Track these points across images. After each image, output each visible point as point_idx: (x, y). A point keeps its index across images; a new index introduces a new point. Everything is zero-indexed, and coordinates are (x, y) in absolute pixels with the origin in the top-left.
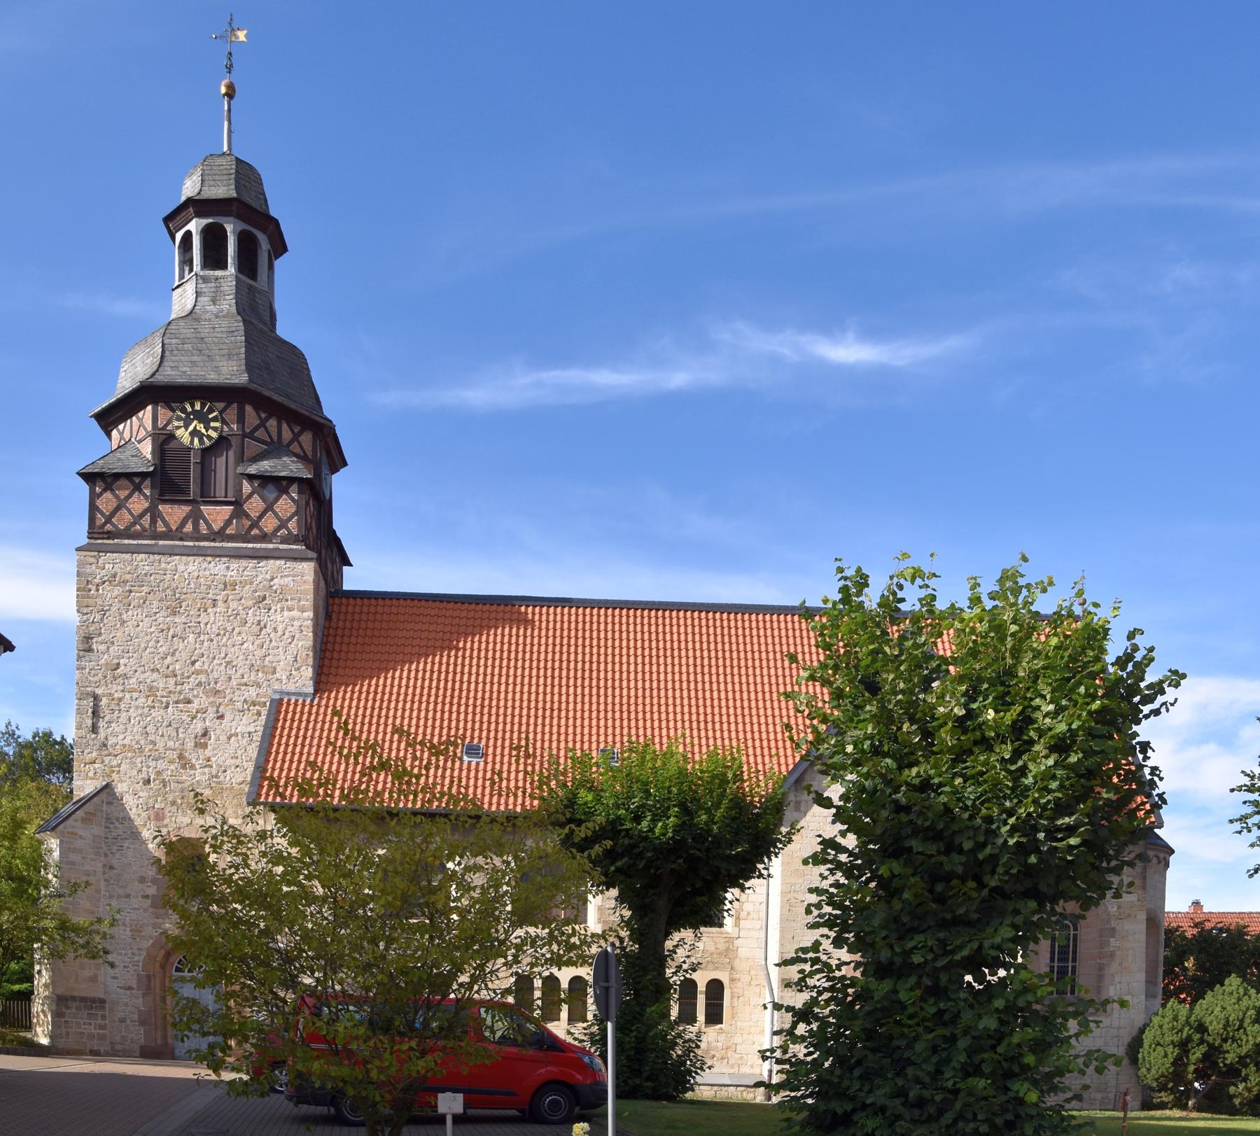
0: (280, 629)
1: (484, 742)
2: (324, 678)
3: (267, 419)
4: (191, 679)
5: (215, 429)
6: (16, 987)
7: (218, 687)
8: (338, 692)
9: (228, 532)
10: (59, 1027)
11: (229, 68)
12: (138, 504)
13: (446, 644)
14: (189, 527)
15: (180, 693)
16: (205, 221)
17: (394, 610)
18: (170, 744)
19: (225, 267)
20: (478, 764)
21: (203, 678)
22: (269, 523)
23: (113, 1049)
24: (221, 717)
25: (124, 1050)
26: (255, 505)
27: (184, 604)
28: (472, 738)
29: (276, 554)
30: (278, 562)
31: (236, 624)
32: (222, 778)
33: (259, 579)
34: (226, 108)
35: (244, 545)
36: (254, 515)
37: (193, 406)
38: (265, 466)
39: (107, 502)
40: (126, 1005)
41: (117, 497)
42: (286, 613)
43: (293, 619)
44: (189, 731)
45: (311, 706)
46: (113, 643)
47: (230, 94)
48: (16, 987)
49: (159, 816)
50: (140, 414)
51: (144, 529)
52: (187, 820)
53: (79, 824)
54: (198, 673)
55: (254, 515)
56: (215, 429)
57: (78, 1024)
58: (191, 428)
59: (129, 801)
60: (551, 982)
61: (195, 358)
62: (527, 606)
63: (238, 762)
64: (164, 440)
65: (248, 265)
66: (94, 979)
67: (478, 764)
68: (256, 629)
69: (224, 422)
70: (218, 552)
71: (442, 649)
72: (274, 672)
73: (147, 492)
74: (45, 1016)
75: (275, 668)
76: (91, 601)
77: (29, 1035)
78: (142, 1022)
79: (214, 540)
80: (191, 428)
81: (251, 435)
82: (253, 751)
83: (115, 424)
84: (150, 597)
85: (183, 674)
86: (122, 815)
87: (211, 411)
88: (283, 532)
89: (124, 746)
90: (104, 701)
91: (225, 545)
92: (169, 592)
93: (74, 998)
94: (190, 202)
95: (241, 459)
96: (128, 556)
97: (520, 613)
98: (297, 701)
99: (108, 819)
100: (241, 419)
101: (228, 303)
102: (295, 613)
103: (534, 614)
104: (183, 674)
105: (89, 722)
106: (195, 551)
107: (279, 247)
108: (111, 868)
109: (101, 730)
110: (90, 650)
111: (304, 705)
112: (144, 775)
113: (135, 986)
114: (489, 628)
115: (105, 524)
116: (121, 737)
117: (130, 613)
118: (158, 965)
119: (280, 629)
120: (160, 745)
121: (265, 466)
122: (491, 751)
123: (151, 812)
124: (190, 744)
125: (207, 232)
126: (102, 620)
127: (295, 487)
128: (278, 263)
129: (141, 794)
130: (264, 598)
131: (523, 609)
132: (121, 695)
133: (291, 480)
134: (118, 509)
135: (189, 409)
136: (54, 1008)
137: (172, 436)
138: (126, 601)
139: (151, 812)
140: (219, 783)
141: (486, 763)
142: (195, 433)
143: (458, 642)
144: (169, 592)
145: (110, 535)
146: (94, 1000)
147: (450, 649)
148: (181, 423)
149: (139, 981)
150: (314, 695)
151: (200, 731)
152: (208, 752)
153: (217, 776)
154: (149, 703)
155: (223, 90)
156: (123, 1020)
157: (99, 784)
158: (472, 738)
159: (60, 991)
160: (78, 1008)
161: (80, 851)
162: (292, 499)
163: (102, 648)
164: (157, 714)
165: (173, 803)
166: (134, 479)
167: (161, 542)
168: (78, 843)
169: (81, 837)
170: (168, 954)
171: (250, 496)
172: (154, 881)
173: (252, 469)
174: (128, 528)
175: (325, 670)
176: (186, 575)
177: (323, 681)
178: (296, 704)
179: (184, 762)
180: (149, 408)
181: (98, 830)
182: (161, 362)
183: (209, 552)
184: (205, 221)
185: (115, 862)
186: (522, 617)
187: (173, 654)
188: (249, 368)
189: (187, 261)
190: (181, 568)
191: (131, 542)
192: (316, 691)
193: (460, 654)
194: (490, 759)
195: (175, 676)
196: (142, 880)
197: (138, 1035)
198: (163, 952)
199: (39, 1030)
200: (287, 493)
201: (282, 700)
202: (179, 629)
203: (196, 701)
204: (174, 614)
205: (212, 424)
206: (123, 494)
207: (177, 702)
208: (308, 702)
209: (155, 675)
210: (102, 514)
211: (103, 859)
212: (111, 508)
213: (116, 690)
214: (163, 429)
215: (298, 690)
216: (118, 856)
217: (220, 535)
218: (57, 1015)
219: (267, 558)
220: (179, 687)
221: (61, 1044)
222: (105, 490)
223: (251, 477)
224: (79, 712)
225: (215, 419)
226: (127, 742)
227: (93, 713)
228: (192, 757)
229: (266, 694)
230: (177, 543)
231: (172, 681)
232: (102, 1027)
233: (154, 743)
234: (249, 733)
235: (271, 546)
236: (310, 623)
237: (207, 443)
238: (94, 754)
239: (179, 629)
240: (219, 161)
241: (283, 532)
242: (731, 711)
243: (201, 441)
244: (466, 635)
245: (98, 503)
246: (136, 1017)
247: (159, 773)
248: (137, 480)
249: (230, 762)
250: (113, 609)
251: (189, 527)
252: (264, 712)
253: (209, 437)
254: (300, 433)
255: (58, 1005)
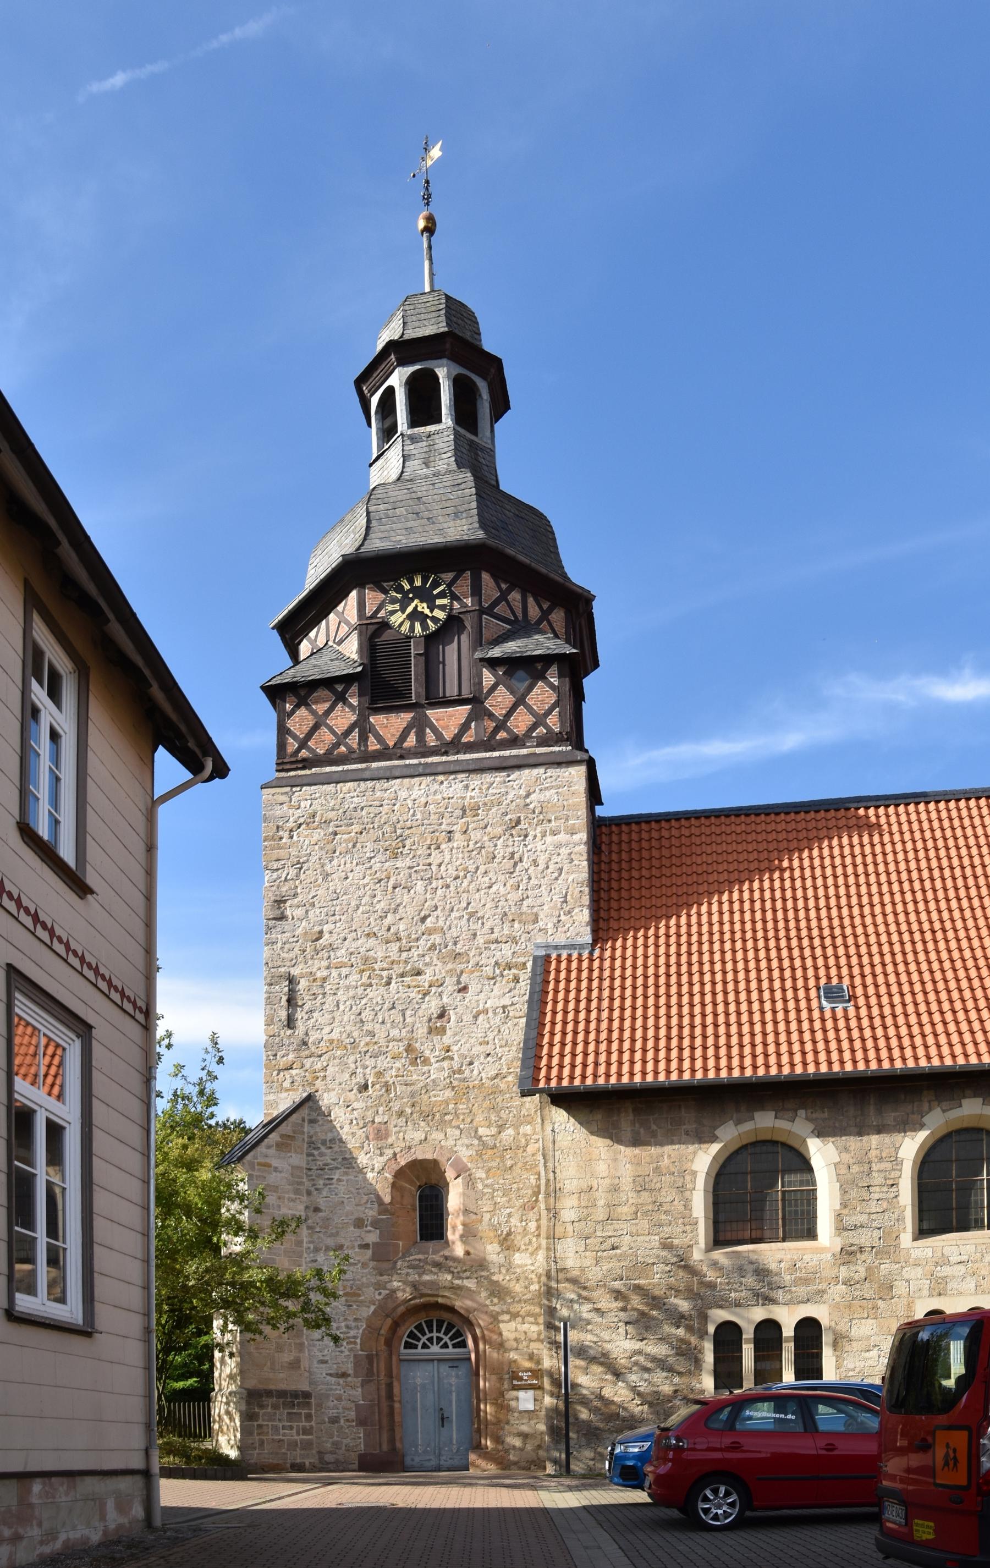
0: (542, 861)
1: (846, 982)
2: (602, 924)
3: (509, 591)
4: (421, 942)
5: (442, 608)
6: (180, 1385)
7: (459, 948)
8: (625, 940)
9: (464, 740)
10: (251, 1434)
11: (427, 199)
12: (343, 718)
13: (765, 863)
14: (411, 741)
15: (406, 962)
16: (409, 370)
17: (685, 832)
18: (395, 1033)
19: (439, 420)
20: (845, 1010)
21: (437, 939)
22: (521, 722)
23: (321, 1460)
24: (464, 989)
25: (337, 1462)
26: (500, 701)
27: (408, 842)
28: (829, 978)
29: (532, 761)
30: (535, 771)
31: (479, 862)
32: (467, 1073)
33: (510, 797)
34: (425, 245)
35: (488, 755)
36: (499, 712)
37: (411, 582)
38: (512, 647)
39: (300, 721)
40: (339, 1398)
41: (314, 713)
42: (549, 839)
43: (559, 846)
44: (420, 1013)
45: (591, 960)
46: (313, 905)
47: (430, 229)
48: (180, 1385)
49: (381, 1134)
50: (340, 608)
51: (351, 751)
52: (420, 1135)
53: (272, 1151)
54: (430, 932)
55: (499, 712)
56: (442, 608)
57: (276, 1428)
58: (410, 609)
59: (340, 1117)
60: (769, 1329)
61: (410, 524)
62: (867, 808)
63: (489, 1048)
64: (373, 632)
65: (466, 416)
66: (295, 1365)
67: (845, 1010)
68: (508, 864)
69: (454, 597)
70: (452, 768)
71: (761, 872)
72: (536, 921)
73: (354, 701)
74: (232, 1419)
75: (536, 915)
76: (282, 853)
77: (207, 1445)
78: (361, 1422)
79: (446, 753)
80: (410, 609)
81: (489, 611)
82: (516, 1032)
83: (304, 632)
84: (362, 838)
85: (409, 936)
86: (330, 1136)
87: (436, 584)
88: (541, 730)
89: (331, 1041)
90: (303, 984)
91: (461, 757)
92: (387, 828)
93: (269, 1393)
94: (391, 346)
95: (478, 642)
96: (330, 788)
97: (859, 818)
98: (570, 955)
99: (311, 1143)
100: (476, 591)
101: (446, 461)
102: (562, 837)
103: (878, 817)
104: (409, 936)
105: (283, 1014)
106: (421, 770)
107: (501, 405)
108: (317, 1210)
109: (299, 1023)
110: (282, 918)
111: (580, 960)
112: (360, 1079)
113: (351, 1372)
114: (820, 840)
115: (299, 750)
116: (327, 1029)
117: (335, 862)
118: (382, 1340)
119: (542, 861)
120: (381, 1034)
121: (512, 647)
122: (859, 991)
123: (370, 1129)
124: (422, 1031)
125: (412, 384)
126: (298, 875)
127: (553, 670)
128: (496, 426)
129: (355, 1105)
130: (518, 822)
131: (861, 812)
132: (325, 973)
133: (548, 660)
134: (316, 727)
135: (407, 587)
136: (244, 1407)
137: (385, 625)
138: (330, 847)
139: (370, 1129)
140: (464, 1080)
141: (857, 1008)
142: (415, 616)
143: (781, 861)
144: (387, 828)
145: (306, 764)
146: (295, 1394)
147: (772, 871)
148: (397, 606)
149: (357, 1364)
150: (593, 945)
151: (435, 1011)
152: (447, 1040)
153: (460, 1071)
154: (364, 979)
155: (421, 224)
156: (334, 1420)
157: (298, 1096)
158: (829, 978)
159: (252, 1384)
160: (275, 1407)
161: (275, 1188)
162: (552, 686)
163: (299, 912)
164: (375, 994)
165: (401, 1114)
166: (334, 686)
167: (374, 765)
168: (273, 1178)
169: (276, 1169)
170: (396, 1325)
171: (493, 688)
172: (375, 1224)
173: (496, 652)
174: (329, 752)
175: (602, 914)
176: (410, 803)
177: (605, 923)
178: (569, 960)
179: (414, 1056)
180: (354, 594)
181: (298, 1159)
182: (367, 534)
183: (440, 769)
184: (409, 370)
185: (322, 1203)
186: (864, 821)
187: (395, 911)
188: (483, 524)
189: (388, 432)
190: (403, 794)
191: (334, 769)
192: (595, 942)
193: (787, 875)
194: (861, 1001)
195: (399, 939)
196: (359, 1223)
197: (355, 1440)
198: (389, 1321)
199: (222, 1439)
200: (543, 678)
201: (549, 956)
202: (402, 878)
203: (429, 971)
204: (395, 856)
205: (438, 602)
206: (321, 708)
207: (402, 975)
208: (586, 954)
209: (372, 942)
210: (295, 737)
211: (305, 1198)
212: (306, 729)
213: (318, 967)
214: (371, 617)
215: (569, 942)
216: (324, 1193)
217: (455, 745)
218: (248, 1417)
219: (519, 767)
220: (404, 955)
221: (255, 1456)
222: (297, 706)
223: (493, 663)
224: (269, 1001)
225: (442, 595)
226: (335, 1035)
227: (289, 1001)
228: (424, 1046)
229: (526, 952)
230: (396, 763)
231: (394, 947)
232: (306, 1431)
233: (372, 1034)
234: (504, 1007)
235: (524, 751)
236: (583, 849)
237: (432, 626)
238: (291, 1056)
239: (402, 878)
240: (424, 298)
241: (541, 730)
242: (868, 1033)
243: (425, 627)
244: (791, 852)
245: (290, 724)
246: (352, 1414)
247: (380, 1074)
248: (340, 688)
249: (478, 1049)
250: (313, 859)
251: (411, 741)
252: (525, 976)
253: (434, 619)
254: (550, 610)
255: (248, 1403)
